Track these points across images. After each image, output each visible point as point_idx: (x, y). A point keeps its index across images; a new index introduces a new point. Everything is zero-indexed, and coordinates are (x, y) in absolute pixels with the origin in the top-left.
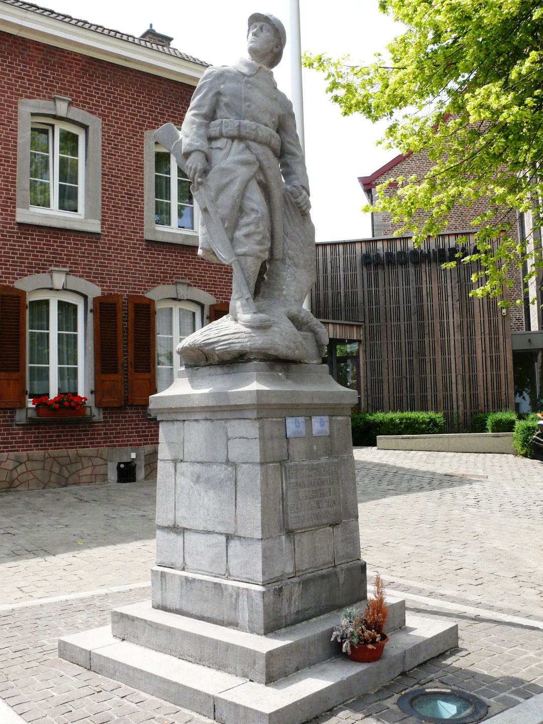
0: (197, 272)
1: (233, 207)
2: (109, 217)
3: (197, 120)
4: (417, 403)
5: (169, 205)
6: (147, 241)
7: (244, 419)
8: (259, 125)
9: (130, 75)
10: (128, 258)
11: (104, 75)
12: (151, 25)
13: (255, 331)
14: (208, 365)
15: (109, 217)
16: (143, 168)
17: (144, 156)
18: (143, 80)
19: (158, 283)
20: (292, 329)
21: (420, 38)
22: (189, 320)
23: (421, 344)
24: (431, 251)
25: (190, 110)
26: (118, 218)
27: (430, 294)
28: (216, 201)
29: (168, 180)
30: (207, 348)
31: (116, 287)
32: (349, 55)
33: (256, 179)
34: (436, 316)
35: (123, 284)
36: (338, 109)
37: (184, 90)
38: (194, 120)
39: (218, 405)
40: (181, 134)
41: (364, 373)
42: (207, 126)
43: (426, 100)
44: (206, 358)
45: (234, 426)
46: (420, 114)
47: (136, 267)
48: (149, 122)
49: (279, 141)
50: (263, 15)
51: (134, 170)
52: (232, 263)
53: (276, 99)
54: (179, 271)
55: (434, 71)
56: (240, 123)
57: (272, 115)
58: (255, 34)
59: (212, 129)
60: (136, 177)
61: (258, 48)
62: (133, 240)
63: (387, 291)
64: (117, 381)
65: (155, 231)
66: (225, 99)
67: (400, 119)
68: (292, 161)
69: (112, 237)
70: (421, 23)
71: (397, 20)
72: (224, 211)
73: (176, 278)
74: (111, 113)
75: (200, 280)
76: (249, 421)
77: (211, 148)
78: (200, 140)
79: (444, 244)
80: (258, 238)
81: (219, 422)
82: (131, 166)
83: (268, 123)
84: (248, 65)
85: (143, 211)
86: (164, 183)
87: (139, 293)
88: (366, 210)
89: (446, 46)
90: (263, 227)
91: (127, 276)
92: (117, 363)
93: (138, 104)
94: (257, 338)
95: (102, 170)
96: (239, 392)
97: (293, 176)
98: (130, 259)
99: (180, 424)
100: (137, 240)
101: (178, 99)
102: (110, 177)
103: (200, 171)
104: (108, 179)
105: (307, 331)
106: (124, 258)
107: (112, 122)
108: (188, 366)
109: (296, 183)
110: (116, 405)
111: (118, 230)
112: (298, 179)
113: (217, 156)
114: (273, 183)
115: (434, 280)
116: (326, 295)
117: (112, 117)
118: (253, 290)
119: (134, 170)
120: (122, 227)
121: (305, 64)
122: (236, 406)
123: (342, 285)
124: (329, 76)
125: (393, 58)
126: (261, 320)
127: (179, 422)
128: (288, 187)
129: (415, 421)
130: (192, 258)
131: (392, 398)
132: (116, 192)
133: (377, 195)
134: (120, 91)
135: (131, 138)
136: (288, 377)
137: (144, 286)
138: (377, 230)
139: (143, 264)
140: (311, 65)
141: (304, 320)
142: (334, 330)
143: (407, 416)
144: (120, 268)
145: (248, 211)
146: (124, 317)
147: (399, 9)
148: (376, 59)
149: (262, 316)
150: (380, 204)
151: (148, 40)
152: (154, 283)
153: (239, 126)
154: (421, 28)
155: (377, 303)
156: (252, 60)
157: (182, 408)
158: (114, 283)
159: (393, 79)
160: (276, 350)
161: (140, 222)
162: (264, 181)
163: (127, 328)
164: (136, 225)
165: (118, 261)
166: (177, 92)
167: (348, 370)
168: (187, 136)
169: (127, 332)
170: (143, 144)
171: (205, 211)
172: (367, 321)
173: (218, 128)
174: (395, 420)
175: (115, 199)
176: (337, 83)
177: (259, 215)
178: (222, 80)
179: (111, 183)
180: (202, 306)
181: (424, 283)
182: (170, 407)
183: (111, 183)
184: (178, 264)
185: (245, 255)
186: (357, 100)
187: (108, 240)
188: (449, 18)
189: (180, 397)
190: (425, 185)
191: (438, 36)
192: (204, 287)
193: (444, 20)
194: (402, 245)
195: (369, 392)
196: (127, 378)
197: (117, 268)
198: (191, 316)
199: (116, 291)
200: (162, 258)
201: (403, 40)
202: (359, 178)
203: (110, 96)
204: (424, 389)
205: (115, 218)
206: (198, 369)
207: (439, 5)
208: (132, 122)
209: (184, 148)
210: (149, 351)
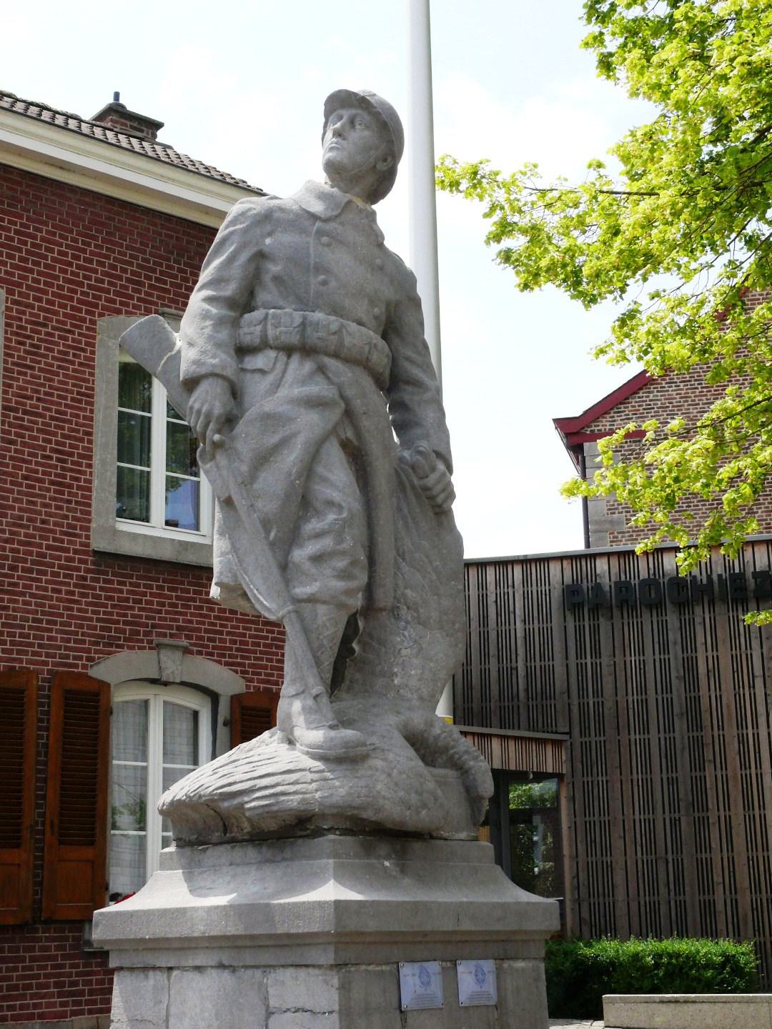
0: (204, 623)
1: (288, 496)
2: (15, 500)
3: (214, 311)
4: (693, 915)
5: (146, 477)
6: (96, 553)
7: (307, 966)
8: (345, 322)
9: (70, 199)
10: (54, 590)
11: (13, 198)
12: (117, 95)
13: (333, 766)
14: (228, 842)
15: (15, 500)
16: (92, 396)
17: (97, 371)
18: (97, 211)
19: (118, 646)
20: (413, 763)
21: (684, 133)
22: (184, 726)
23: (698, 785)
24: (715, 577)
25: (199, 290)
26: (34, 503)
27: (714, 672)
28: (251, 484)
29: (146, 424)
30: (226, 804)
31: (26, 653)
32: (535, 166)
33: (338, 436)
34: (730, 719)
35: (40, 646)
36: (510, 277)
37: (185, 233)
38: (208, 311)
39: (248, 933)
40: (179, 340)
41: (570, 846)
42: (235, 323)
43: (700, 261)
44: (224, 825)
45: (283, 983)
46: (688, 290)
47: (71, 609)
48: (108, 300)
49: (387, 356)
50: (355, 94)
51: (73, 400)
52: (283, 617)
53: (381, 268)
54: (165, 619)
55: (717, 199)
56: (305, 318)
57: (372, 303)
58: (338, 134)
59: (246, 330)
60: (77, 416)
61: (346, 161)
62: (67, 550)
63: (620, 666)
64: (19, 865)
65: (116, 532)
66: (274, 268)
67: (645, 302)
68: (416, 398)
69: (21, 543)
70: (686, 102)
71: (635, 94)
72: (268, 506)
73: (159, 635)
74: (26, 278)
75: (210, 640)
76: (316, 971)
77: (243, 370)
78: (219, 352)
79: (743, 564)
80: (341, 563)
81: (250, 972)
82: (67, 391)
83: (365, 319)
84: (322, 196)
85: (90, 490)
86: (137, 432)
87: (76, 666)
88: (571, 492)
89: (741, 147)
90: (352, 541)
91: (50, 630)
92: (19, 825)
93: (85, 260)
94: (337, 784)
95: (4, 400)
96: (289, 904)
97: (418, 431)
98: (59, 591)
99: (160, 977)
100: (76, 552)
101: (173, 253)
102: (20, 415)
103: (218, 418)
104: (16, 418)
105: (445, 767)
106: (46, 589)
107: (28, 297)
108: (182, 843)
109: (424, 445)
110: (11, 921)
111: (35, 528)
112: (427, 436)
113: (256, 388)
114: (374, 446)
115: (724, 641)
116: (484, 674)
117: (28, 287)
118: (329, 676)
119: (73, 400)
120: (43, 522)
121: (443, 182)
122: (289, 936)
123: (521, 651)
124: (493, 208)
125: (628, 173)
126: (346, 743)
127: (158, 973)
128: (406, 454)
129: (691, 960)
130: (195, 592)
131: (634, 906)
132: (33, 447)
133: (598, 459)
134: (48, 232)
135: (69, 332)
136: (403, 870)
137: (88, 651)
138: (596, 532)
139: (88, 604)
140: (454, 185)
141: (440, 744)
142: (505, 751)
143: (670, 949)
144: (37, 612)
145: (318, 505)
146: (40, 720)
147: (641, 74)
148: (593, 175)
149: (348, 733)
150: (604, 480)
151: (109, 125)
152: (111, 645)
153: (303, 325)
154: (686, 112)
155: (598, 692)
156: (332, 187)
157: (167, 939)
158: (21, 644)
159: (630, 218)
160: (378, 810)
161: (82, 512)
162: (356, 443)
163: (46, 745)
164: (74, 518)
165: (32, 595)
166: (170, 237)
167: (535, 838)
168: (191, 344)
169: (46, 754)
170: (93, 345)
171: (228, 503)
172: (576, 731)
173: (259, 328)
174: (643, 957)
175: (30, 462)
176: (510, 224)
177: (345, 515)
178: (268, 228)
179: (21, 427)
180: (214, 697)
181: (701, 648)
182: (140, 936)
183: (21, 427)
184: (163, 605)
185: (312, 600)
186: (552, 259)
187: (12, 550)
188: (746, 91)
189: (164, 913)
190: (703, 441)
191: (723, 129)
192: (219, 655)
193: (736, 96)
194: (651, 565)
195: (583, 890)
196: (42, 858)
197: (28, 611)
198: (190, 717)
199: (25, 661)
200: (129, 592)
201: (649, 136)
202: (555, 421)
203: (25, 243)
204: (706, 886)
205: (29, 502)
206: (204, 850)
207: (723, 65)
208: (71, 299)
209: (185, 368)
210: (94, 797)
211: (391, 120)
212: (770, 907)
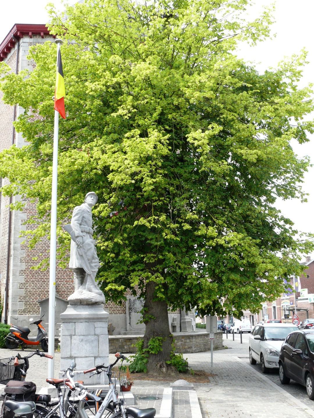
211: (242, 67)
212: (3, 293)
